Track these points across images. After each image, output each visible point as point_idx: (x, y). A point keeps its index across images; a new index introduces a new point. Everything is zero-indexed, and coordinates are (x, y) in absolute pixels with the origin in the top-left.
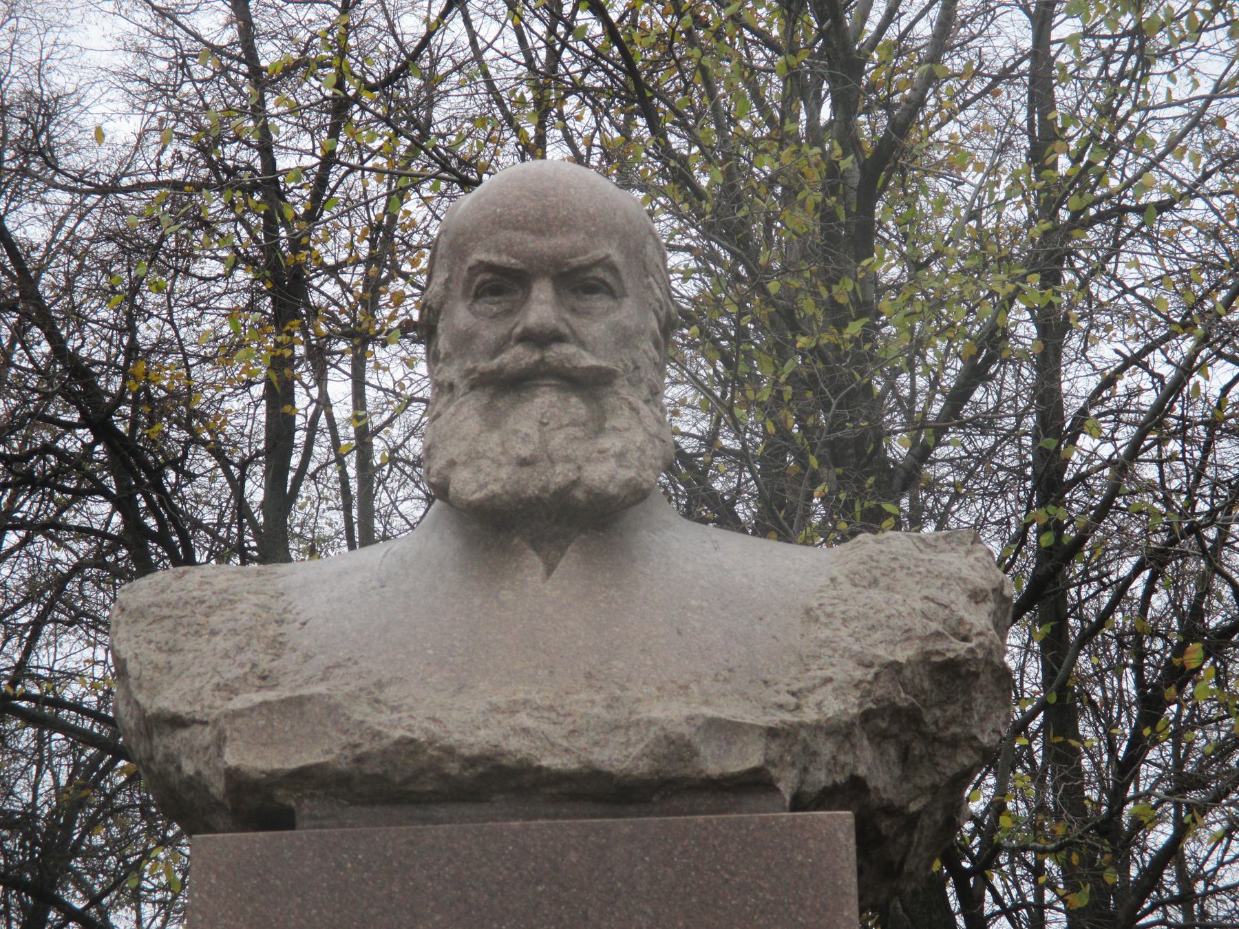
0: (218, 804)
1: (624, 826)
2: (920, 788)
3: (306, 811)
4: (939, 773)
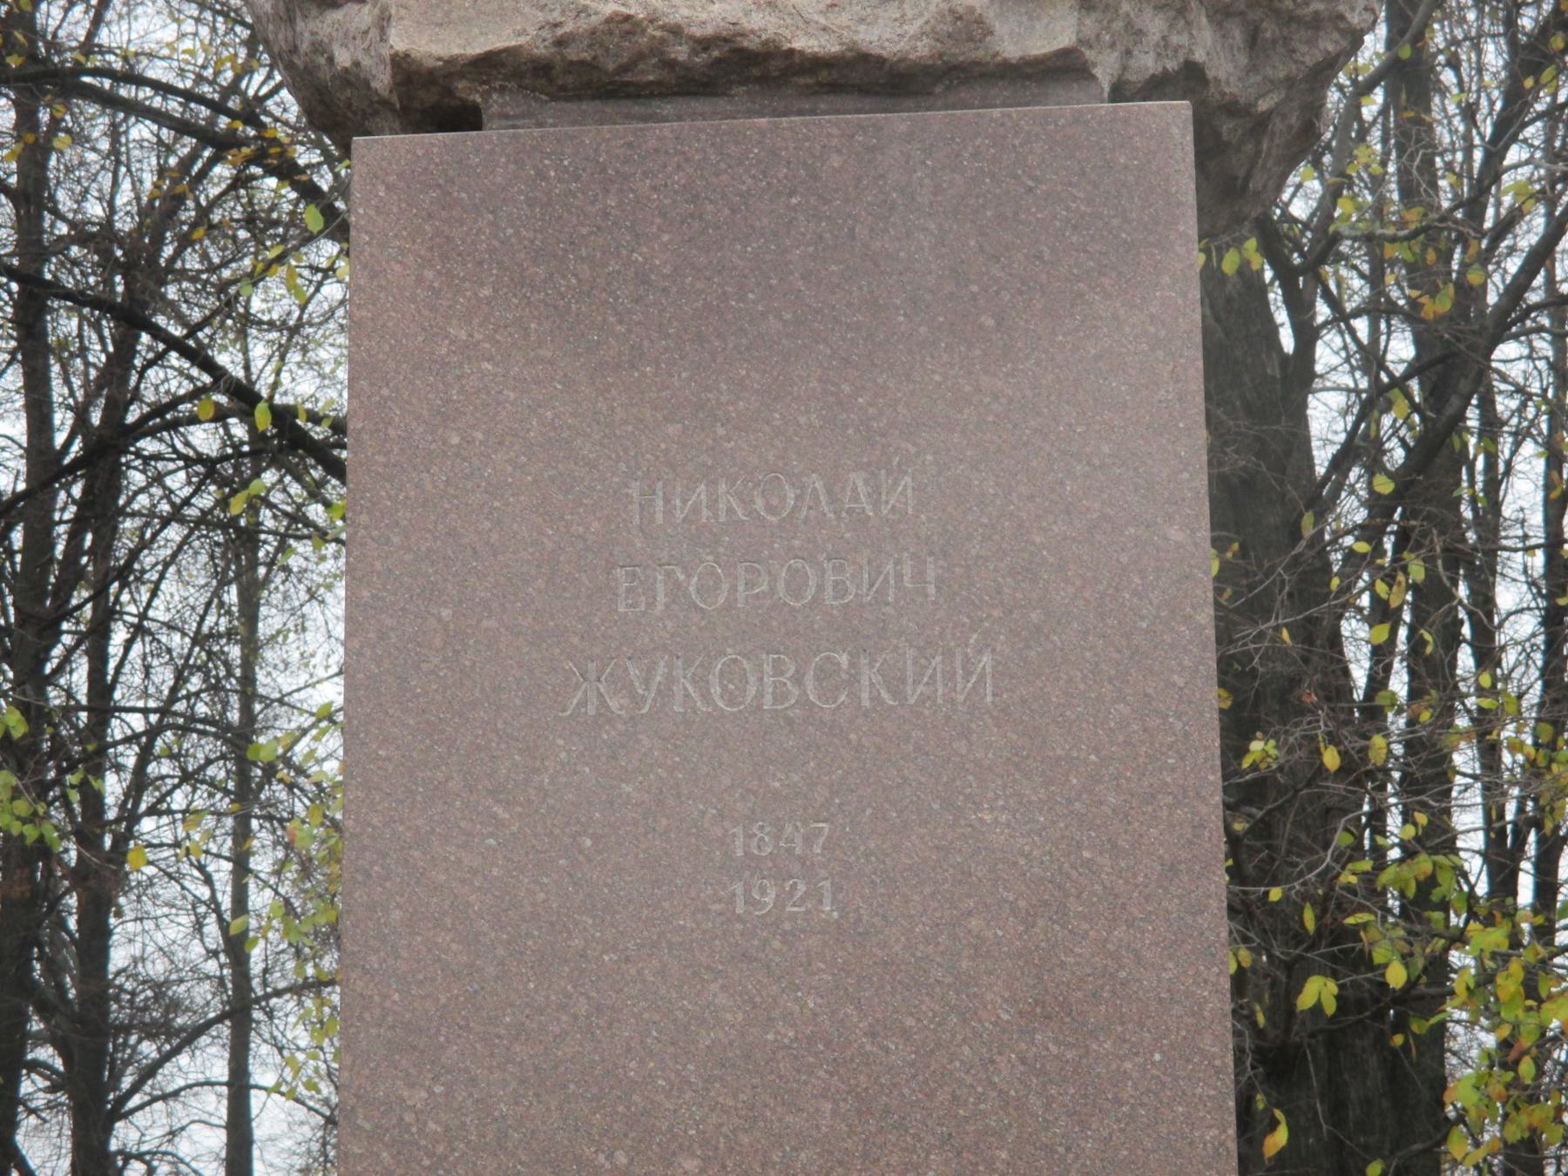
0: (384, 102)
1: (899, 122)
2: (1271, 81)
3: (495, 108)
4: (1296, 62)
